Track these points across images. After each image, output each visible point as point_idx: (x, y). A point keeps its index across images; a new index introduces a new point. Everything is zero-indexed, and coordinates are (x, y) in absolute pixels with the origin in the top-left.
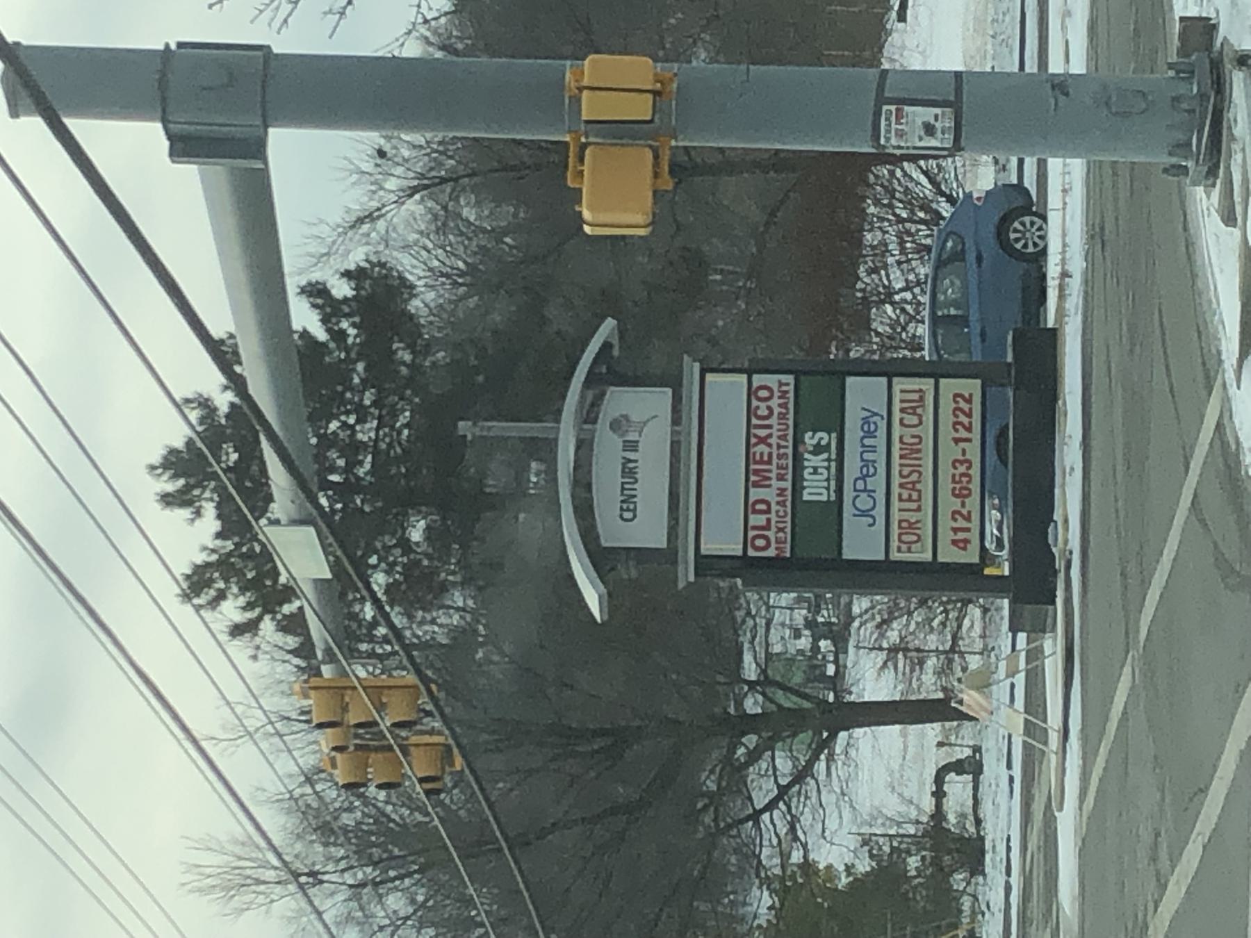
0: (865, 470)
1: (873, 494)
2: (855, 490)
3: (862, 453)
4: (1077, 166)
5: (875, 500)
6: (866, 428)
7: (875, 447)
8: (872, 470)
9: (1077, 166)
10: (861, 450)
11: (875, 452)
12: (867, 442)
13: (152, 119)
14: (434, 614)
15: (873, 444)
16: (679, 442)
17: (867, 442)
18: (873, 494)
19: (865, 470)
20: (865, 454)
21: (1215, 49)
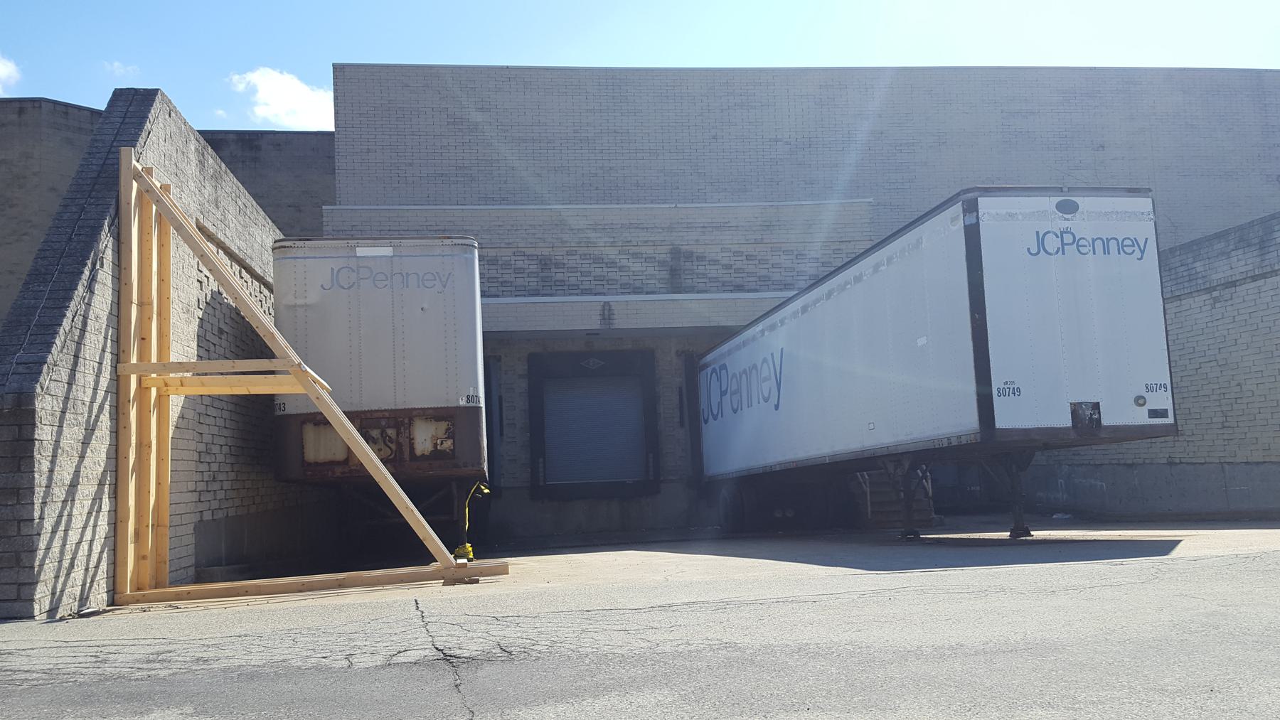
7: (1109, 253)
11: (1105, 253)
12: (1113, 244)
17: (1113, 243)
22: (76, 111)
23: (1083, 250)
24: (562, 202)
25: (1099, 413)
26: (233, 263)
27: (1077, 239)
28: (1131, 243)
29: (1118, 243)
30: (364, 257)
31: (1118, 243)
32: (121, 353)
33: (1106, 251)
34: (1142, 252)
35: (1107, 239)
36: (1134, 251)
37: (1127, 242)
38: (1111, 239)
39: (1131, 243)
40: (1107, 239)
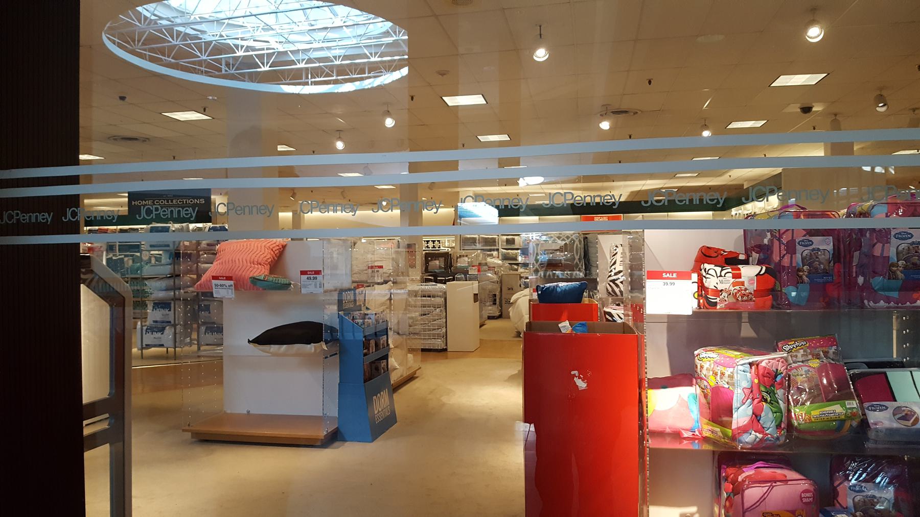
0: (239, 208)
1: (243, 214)
2: (392, 199)
3: (499, 199)
4: (279, 146)
5: (239, 214)
6: (263, 208)
7: (252, 214)
8: (238, 212)
9: (279, 146)
10: (250, 205)
11: (250, 214)
12: (254, 209)
13: (398, 209)
14: (723, 440)
15: (254, 213)
16: (267, 48)
17: (254, 209)
18: (243, 214)
19: (239, 208)
20: (248, 208)
21: (741, 348)
22: (96, 292)
23: (238, 212)
24: (916, 205)
25: (97, 275)
26: (145, 6)
27: (235, 207)
28: (610, 198)
29: (249, 208)
30: (124, 392)
31: (249, 208)
32: (191, 428)
33: (251, 212)
34: (270, 213)
35: (244, 206)
36: (266, 212)
37: (263, 208)
38: (587, 196)
39: (610, 198)
40: (503, 199)
